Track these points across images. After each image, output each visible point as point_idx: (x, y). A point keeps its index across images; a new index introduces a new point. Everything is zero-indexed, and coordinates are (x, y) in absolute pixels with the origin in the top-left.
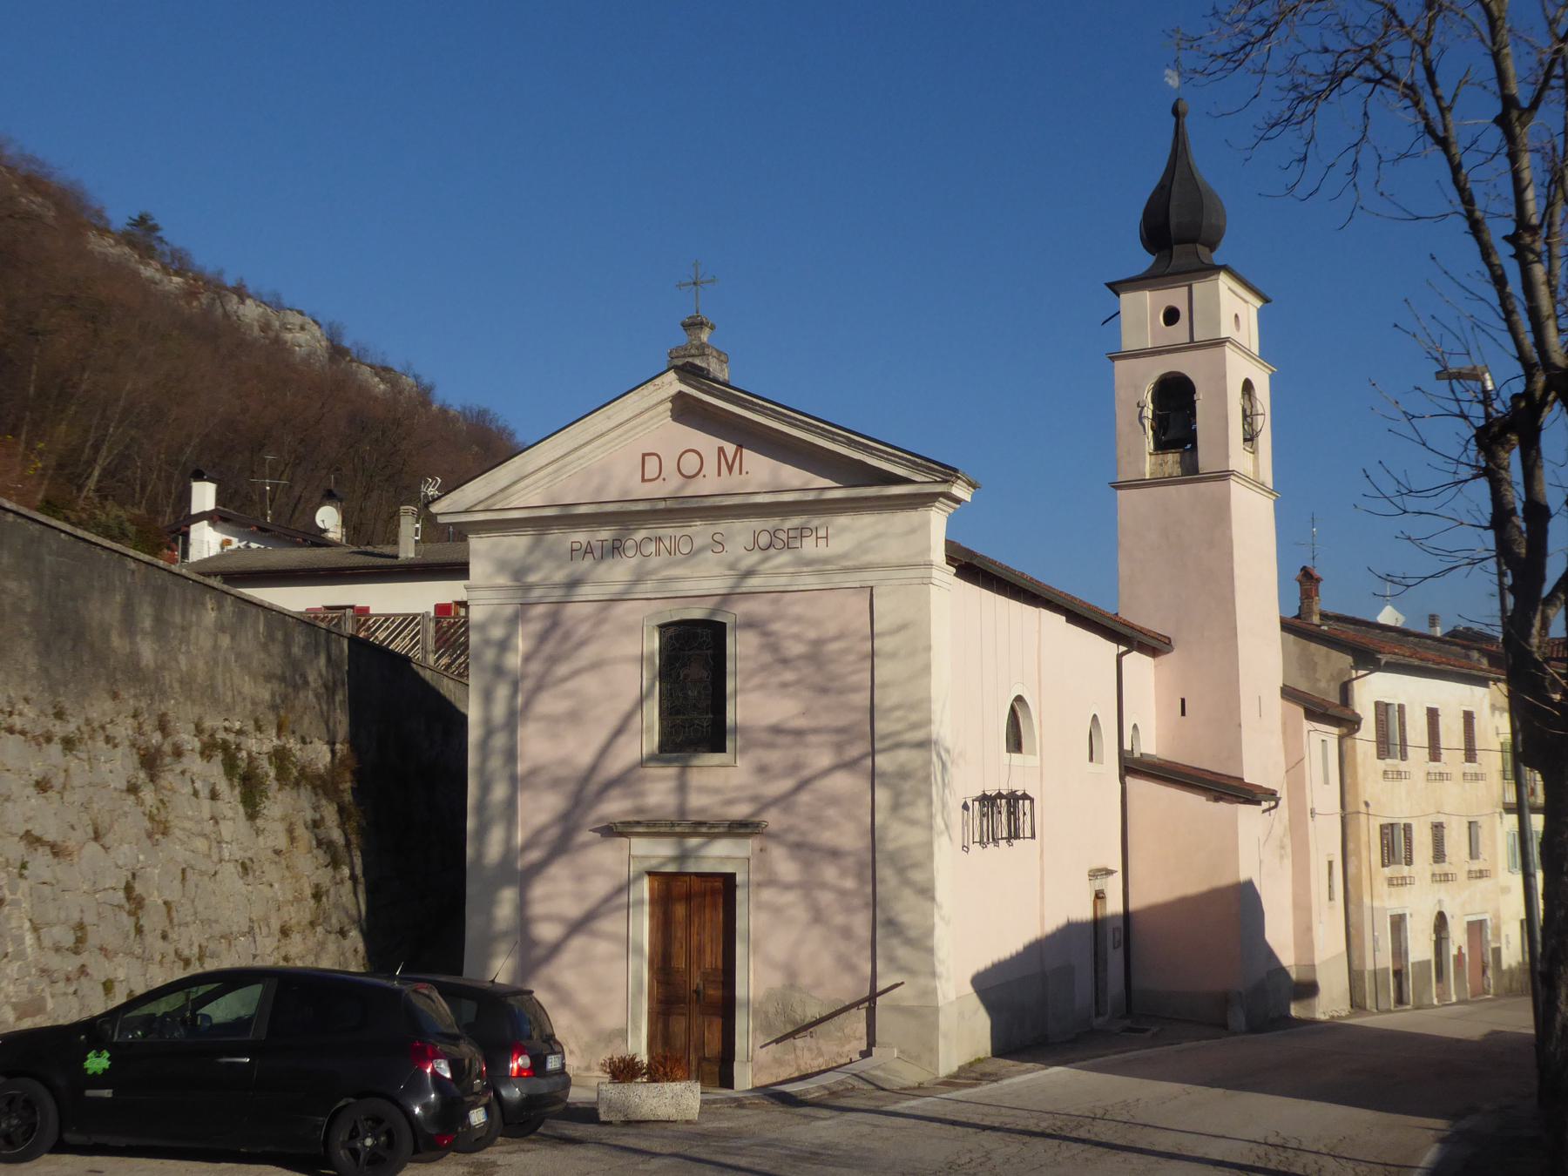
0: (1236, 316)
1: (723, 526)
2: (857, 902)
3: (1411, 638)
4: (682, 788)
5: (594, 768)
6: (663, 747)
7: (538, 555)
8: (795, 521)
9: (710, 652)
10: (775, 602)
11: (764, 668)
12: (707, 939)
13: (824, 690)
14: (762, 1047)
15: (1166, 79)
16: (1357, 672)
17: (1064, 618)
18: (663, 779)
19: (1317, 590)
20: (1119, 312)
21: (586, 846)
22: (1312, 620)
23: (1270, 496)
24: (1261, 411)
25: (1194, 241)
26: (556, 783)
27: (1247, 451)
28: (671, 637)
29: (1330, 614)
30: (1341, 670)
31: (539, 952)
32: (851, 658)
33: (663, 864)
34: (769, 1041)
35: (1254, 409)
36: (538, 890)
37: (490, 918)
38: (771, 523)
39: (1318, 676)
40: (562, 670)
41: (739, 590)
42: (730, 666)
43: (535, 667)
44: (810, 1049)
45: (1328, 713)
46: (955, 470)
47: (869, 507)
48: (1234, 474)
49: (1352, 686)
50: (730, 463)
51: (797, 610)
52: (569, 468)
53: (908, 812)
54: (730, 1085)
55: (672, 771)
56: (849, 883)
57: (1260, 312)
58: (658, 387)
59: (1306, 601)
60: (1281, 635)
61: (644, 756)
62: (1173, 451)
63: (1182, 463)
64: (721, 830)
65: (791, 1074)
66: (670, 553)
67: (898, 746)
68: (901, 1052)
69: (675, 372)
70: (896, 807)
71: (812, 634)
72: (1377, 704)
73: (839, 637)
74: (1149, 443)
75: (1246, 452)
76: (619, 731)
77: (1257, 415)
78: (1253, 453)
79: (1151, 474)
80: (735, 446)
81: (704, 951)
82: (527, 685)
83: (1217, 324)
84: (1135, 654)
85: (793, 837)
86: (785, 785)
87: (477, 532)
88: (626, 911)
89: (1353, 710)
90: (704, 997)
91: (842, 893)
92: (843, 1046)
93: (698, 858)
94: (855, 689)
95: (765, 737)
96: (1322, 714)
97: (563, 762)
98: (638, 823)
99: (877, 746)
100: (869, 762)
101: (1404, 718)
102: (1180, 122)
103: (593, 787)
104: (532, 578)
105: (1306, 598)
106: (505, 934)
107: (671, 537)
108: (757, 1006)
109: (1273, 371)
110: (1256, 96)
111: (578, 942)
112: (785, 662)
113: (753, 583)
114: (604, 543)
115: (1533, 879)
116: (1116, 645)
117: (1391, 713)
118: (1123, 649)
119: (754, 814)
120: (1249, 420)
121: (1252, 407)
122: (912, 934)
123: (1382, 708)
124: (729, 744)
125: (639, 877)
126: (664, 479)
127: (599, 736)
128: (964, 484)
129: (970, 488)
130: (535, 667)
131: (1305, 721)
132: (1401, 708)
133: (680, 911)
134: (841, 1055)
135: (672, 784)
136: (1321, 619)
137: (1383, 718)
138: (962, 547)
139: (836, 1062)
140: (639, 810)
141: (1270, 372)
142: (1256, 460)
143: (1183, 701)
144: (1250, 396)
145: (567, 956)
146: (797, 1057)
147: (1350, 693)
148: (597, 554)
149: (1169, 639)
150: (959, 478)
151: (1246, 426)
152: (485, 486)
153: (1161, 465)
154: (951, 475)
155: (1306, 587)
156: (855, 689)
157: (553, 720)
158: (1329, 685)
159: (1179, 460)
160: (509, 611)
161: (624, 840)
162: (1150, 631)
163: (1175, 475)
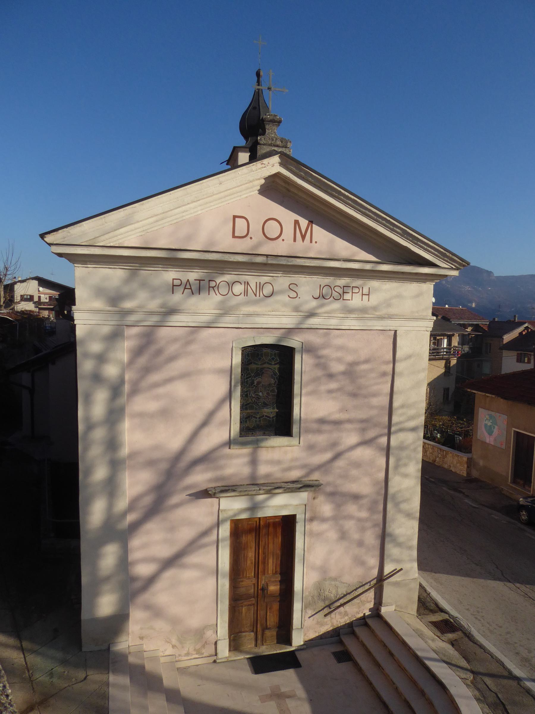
4: (254, 462)
7: (135, 285)
8: (342, 281)
10: (326, 335)
14: (309, 618)
26: (151, 463)
32: (373, 375)
34: (314, 613)
36: (135, 542)
38: (327, 280)
40: (155, 377)
47: (388, 277)
50: (303, 233)
51: (339, 342)
54: (289, 642)
55: (246, 451)
56: (364, 514)
65: (327, 629)
66: (256, 295)
69: (280, 157)
71: (350, 358)
76: (205, 424)
80: (307, 222)
85: (329, 489)
91: (360, 520)
95: (315, 426)
97: (156, 447)
100: (384, 440)
104: (128, 305)
107: (245, 282)
111: (169, 574)
112: (331, 376)
113: (314, 322)
115: (262, 433)
122: (401, 540)
126: (283, 240)
127: (187, 429)
135: (246, 460)
145: (159, 585)
152: (106, 227)
157: (141, 415)
160: (106, 330)
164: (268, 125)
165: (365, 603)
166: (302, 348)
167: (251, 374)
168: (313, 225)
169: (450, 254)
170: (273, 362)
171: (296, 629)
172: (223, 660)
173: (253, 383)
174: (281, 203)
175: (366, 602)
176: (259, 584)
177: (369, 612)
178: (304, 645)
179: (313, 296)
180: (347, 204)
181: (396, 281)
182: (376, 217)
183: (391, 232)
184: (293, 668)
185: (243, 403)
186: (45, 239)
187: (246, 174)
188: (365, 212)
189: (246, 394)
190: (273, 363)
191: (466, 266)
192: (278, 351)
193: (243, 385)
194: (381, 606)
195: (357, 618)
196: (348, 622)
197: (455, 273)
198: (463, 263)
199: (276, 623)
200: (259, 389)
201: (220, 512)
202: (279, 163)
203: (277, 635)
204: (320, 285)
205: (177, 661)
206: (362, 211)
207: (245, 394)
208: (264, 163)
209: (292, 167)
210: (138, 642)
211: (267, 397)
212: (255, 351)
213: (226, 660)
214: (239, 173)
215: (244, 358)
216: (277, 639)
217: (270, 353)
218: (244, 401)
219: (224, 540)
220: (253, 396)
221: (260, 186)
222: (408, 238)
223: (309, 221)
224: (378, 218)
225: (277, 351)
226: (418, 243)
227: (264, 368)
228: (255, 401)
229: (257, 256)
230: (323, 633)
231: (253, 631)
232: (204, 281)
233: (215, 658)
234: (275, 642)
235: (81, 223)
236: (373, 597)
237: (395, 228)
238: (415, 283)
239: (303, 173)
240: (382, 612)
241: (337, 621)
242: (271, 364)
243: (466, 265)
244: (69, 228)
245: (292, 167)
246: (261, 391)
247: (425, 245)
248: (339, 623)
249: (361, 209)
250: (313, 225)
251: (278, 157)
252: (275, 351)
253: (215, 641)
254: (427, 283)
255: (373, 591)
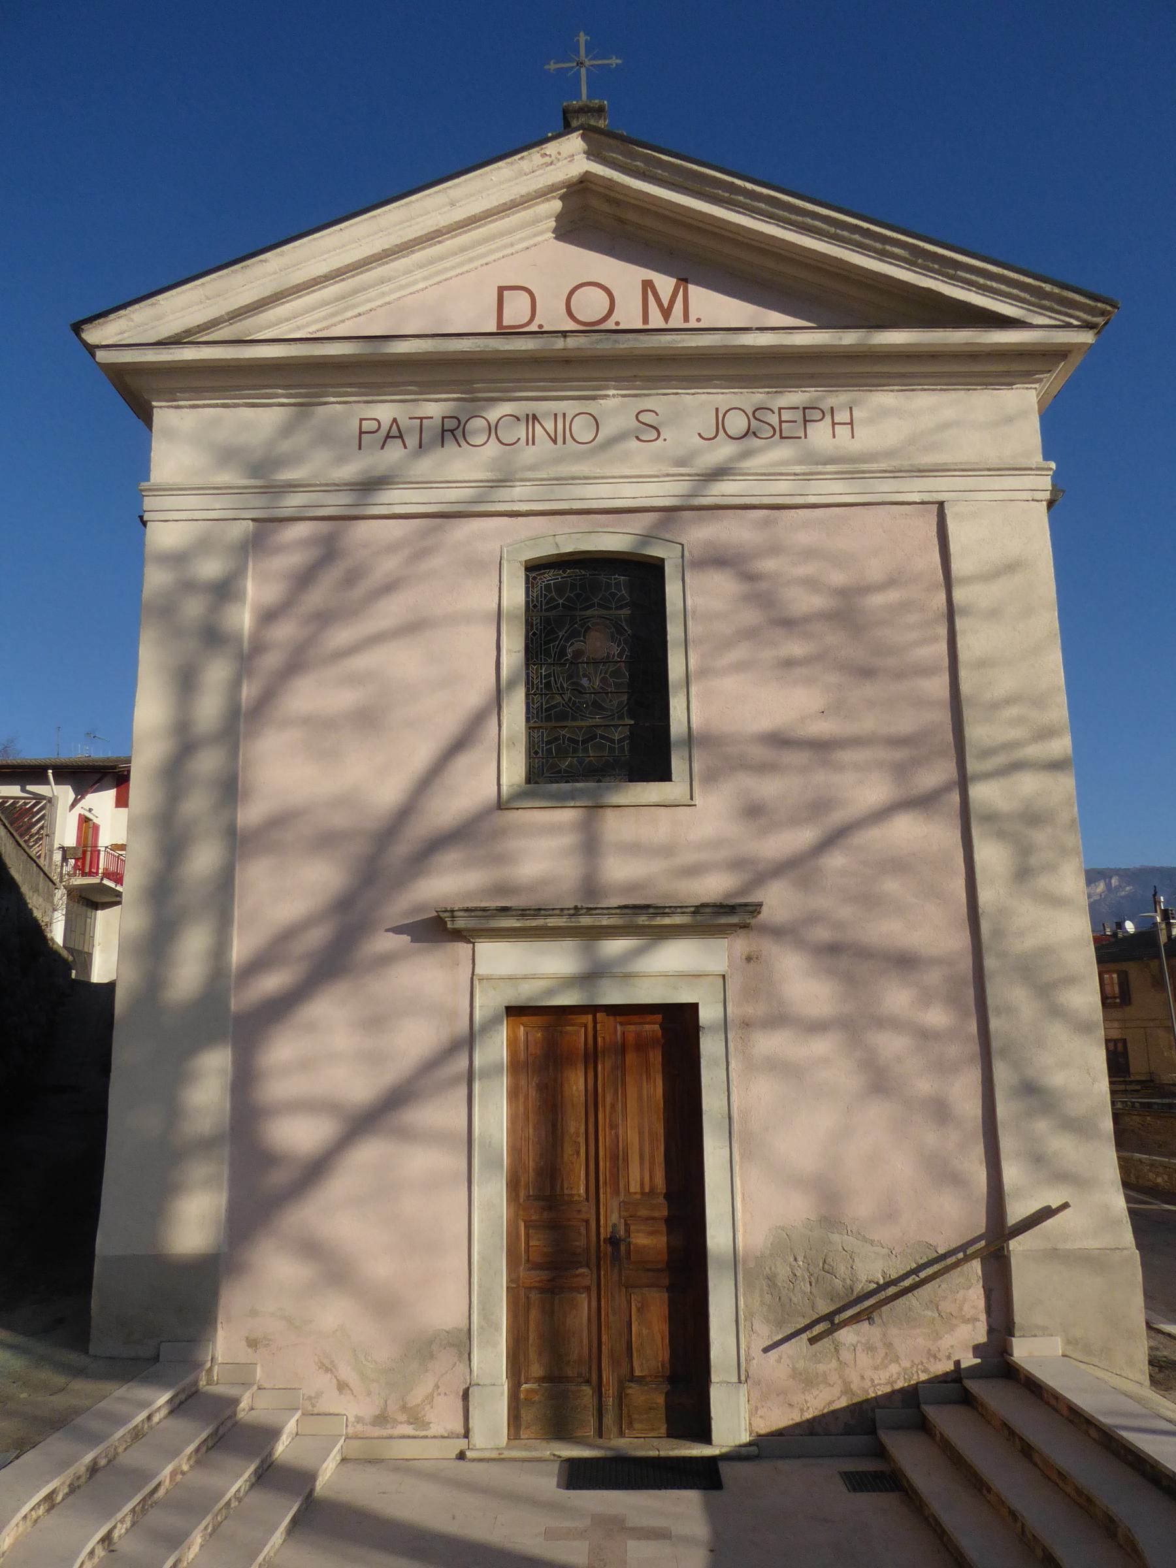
1: (660, 402)
2: (954, 1051)
5: (405, 813)
6: (534, 775)
7: (301, 438)
9: (626, 612)
11: (751, 634)
12: (633, 1137)
13: (866, 673)
14: (766, 1350)
18: (554, 829)
21: (387, 960)
28: (548, 587)
31: (279, 1178)
32: (913, 618)
33: (550, 992)
34: (780, 1337)
37: (173, 1111)
40: (341, 636)
41: (698, 501)
42: (674, 631)
43: (285, 631)
44: (870, 1348)
51: (804, 538)
52: (361, 297)
53: (1044, 882)
54: (705, 1436)
55: (567, 816)
56: (937, 1017)
58: (547, 159)
61: (505, 789)
64: (678, 920)
67: (1017, 766)
68: (1068, 1342)
69: (583, 137)
70: (1023, 874)
71: (838, 578)
73: (890, 583)
76: (460, 744)
81: (626, 1161)
82: (271, 661)
85: (822, 934)
86: (804, 837)
87: (171, 395)
88: (464, 1091)
90: (628, 1252)
91: (925, 1035)
92: (938, 1337)
93: (628, 976)
94: (924, 671)
95: (759, 753)
97: (342, 801)
98: (504, 910)
99: (972, 766)
100: (955, 797)
103: (402, 849)
106: (207, 1145)
107: (556, 415)
108: (752, 1264)
112: (788, 623)
113: (726, 490)
114: (424, 420)
119: (747, 888)
124: (678, 764)
125: (490, 1024)
130: (285, 631)
133: (576, 1083)
134: (935, 1357)
135: (569, 840)
139: (925, 1371)
140: (501, 889)
146: (843, 1364)
148: (412, 441)
156: (924, 671)
160: (240, 530)
161: (463, 948)
164: (576, 119)
165: (954, 1321)
166: (683, 556)
167: (557, 633)
168: (689, 285)
169: (1055, 288)
170: (613, 604)
171: (721, 1383)
172: (487, 1455)
173: (563, 653)
174: (610, 251)
175: (956, 1318)
176: (602, 1222)
177: (975, 1357)
178: (750, 1444)
179: (699, 434)
180: (756, 213)
181: (926, 387)
182: (832, 230)
183: (881, 260)
184: (698, 1488)
185: (539, 704)
186: (84, 336)
187: (510, 180)
188: (803, 223)
189: (545, 683)
190: (614, 606)
191: (1109, 313)
192: (626, 576)
193: (537, 659)
194: (1014, 1336)
195: (932, 1375)
196: (900, 1384)
197: (1087, 337)
198: (1099, 305)
199: (660, 1364)
200: (581, 670)
201: (476, 983)
202: (585, 153)
203: (669, 1407)
204: (717, 409)
205: (350, 1436)
206: (796, 221)
207: (544, 681)
208: (548, 153)
209: (614, 155)
210: (244, 1354)
211: (601, 688)
212: (565, 577)
213: (494, 1455)
214: (493, 178)
215: (537, 596)
216: (669, 1420)
217: (606, 581)
218: (542, 699)
219: (491, 1072)
220: (565, 686)
221: (554, 219)
222: (929, 267)
223: (679, 279)
224: (838, 231)
225: (623, 578)
226: (959, 273)
227: (591, 617)
228: (570, 699)
229: (541, 335)
230: (817, 1413)
231: (588, 1382)
232: (431, 420)
233: (462, 1444)
234: (663, 1430)
235: (155, 298)
236: (981, 1303)
237: (888, 248)
238: (979, 387)
239: (640, 162)
240: (1015, 1355)
241: (862, 1377)
242: (611, 609)
243: (1109, 308)
244: (129, 309)
245: (614, 155)
246: (585, 676)
247: (977, 276)
248: (869, 1384)
249: (793, 217)
250: (689, 285)
251: (580, 138)
252: (617, 576)
253: (464, 1387)
254: (1014, 387)
255: (978, 1281)
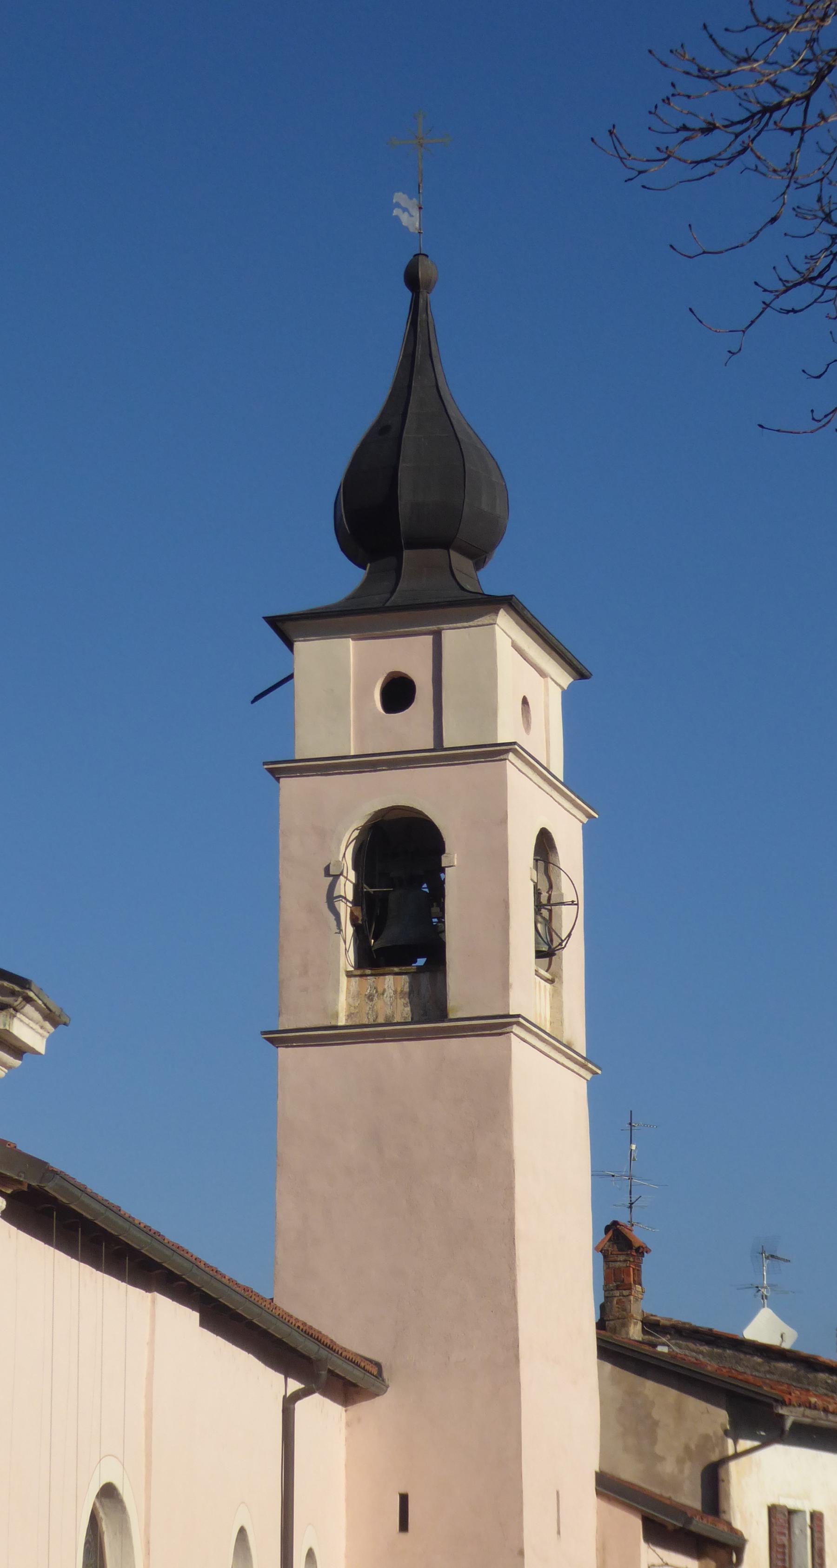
0: (525, 701)
3: (822, 1376)
15: (396, 212)
16: (735, 1443)
17: (196, 1316)
19: (638, 1272)
20: (291, 677)
22: (627, 1333)
23: (583, 1072)
24: (569, 896)
25: (446, 545)
27: (541, 977)
29: (663, 1322)
30: (706, 1438)
35: (554, 893)
39: (659, 1449)
45: (693, 1528)
46: (24, 983)
48: (519, 1024)
49: (727, 1473)
57: (567, 696)
59: (617, 1293)
60: (598, 1362)
62: (396, 969)
63: (413, 994)
72: (773, 1510)
74: (346, 951)
75: (538, 979)
77: (563, 904)
78: (551, 981)
79: (349, 1016)
83: (490, 711)
84: (316, 1398)
89: (729, 1524)
96: (681, 1529)
101: (822, 1540)
102: (421, 301)
105: (617, 1288)
109: (589, 816)
110: (774, 220)
116: (282, 1377)
117: (796, 1530)
118: (295, 1385)
120: (545, 913)
121: (551, 887)
123: (781, 1519)
128: (37, 1016)
129: (47, 1025)
131: (643, 1545)
132: (817, 1518)
136: (644, 1332)
137: (785, 1540)
138: (20, 1153)
141: (585, 820)
142: (557, 995)
143: (404, 1500)
144: (547, 863)
147: (722, 1485)
149: (378, 1365)
150: (28, 1000)
151: (539, 926)
153: (370, 997)
154: (13, 993)
155: (618, 1264)
158: (681, 1471)
159: (407, 989)
162: (345, 1350)
163: (398, 1019)
